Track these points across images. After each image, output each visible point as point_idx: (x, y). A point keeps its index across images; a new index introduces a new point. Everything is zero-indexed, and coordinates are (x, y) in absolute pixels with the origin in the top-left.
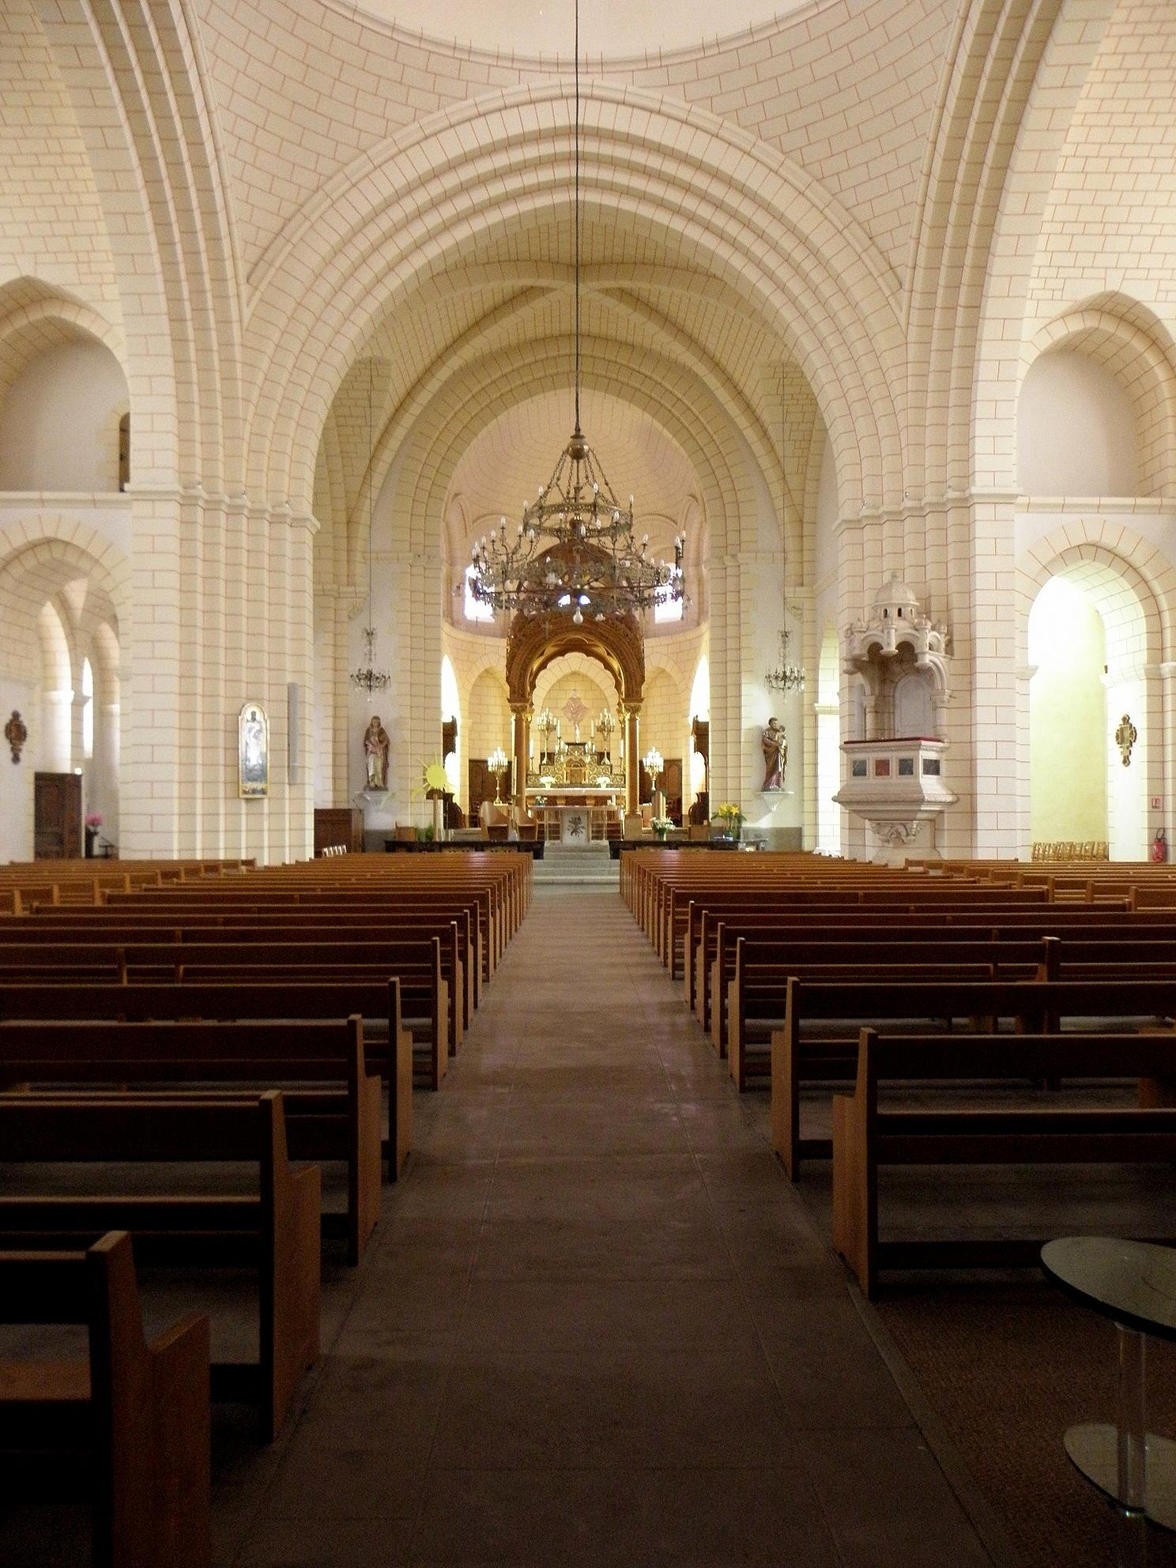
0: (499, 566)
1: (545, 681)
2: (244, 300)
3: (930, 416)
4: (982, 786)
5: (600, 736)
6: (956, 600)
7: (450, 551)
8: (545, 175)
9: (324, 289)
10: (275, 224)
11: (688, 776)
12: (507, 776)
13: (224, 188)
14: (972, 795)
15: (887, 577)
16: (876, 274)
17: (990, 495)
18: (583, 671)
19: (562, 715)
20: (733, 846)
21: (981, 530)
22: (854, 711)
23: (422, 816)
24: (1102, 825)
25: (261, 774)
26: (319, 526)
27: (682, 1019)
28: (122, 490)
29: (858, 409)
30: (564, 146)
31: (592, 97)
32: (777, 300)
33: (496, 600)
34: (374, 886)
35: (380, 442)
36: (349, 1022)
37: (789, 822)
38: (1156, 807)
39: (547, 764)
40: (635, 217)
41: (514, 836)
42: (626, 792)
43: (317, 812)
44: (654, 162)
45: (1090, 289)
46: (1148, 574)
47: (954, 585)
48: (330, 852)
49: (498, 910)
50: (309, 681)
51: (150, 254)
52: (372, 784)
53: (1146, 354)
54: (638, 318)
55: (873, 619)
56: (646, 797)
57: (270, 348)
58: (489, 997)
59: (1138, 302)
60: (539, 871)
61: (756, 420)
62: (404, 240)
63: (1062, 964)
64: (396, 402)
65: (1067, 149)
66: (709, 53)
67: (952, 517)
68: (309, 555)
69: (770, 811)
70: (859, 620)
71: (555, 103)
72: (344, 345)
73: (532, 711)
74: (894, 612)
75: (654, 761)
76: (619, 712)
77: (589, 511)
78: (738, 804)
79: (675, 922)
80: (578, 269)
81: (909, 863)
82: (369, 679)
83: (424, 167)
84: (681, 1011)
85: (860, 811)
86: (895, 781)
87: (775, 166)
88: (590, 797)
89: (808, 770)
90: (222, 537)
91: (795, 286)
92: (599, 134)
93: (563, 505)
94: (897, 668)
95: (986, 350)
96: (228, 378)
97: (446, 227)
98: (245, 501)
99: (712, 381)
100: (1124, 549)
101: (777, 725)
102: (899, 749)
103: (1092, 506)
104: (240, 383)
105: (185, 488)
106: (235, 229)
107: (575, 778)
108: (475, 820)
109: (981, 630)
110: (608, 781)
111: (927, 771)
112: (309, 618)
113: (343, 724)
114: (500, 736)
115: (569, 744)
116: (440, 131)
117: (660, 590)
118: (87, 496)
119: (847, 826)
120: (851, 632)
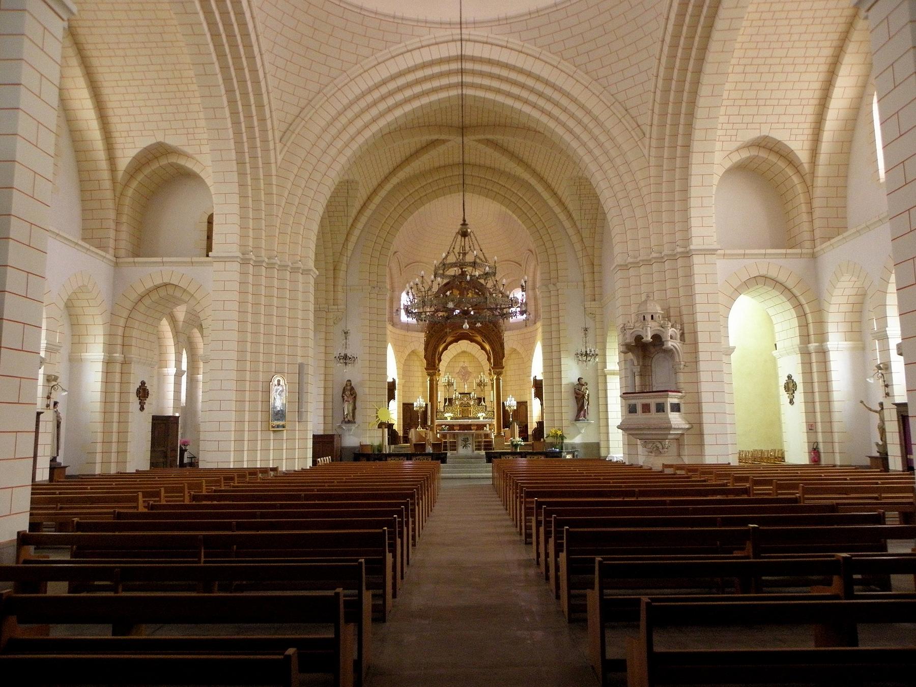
1: (447, 357)
3: (665, 206)
4: (707, 418)
5: (479, 388)
6: (685, 310)
7: (392, 283)
8: (445, 81)
9: (322, 145)
10: (296, 111)
11: (531, 411)
12: (425, 412)
13: (261, 55)
14: (700, 424)
15: (644, 298)
16: (630, 129)
17: (701, 250)
18: (468, 350)
19: (457, 376)
20: (558, 455)
21: (697, 269)
22: (627, 375)
23: (374, 438)
24: (780, 440)
25: (280, 415)
27: (532, 572)
28: (207, 256)
29: (623, 203)
30: (454, 66)
31: (469, 40)
32: (575, 144)
33: (418, 316)
36: (335, 593)
37: (592, 439)
38: (811, 429)
39: (448, 406)
40: (494, 102)
41: (429, 450)
42: (495, 422)
43: (314, 436)
44: (504, 73)
45: (752, 134)
46: (796, 292)
47: (683, 301)
48: (321, 461)
49: (421, 501)
50: (311, 361)
51: (219, 86)
52: (346, 420)
54: (497, 154)
55: (637, 321)
56: (507, 424)
57: (292, 177)
58: (416, 556)
59: (779, 141)
60: (445, 470)
62: (367, 117)
63: (764, 578)
64: (362, 203)
65: (734, 61)
66: (532, 16)
67: (680, 262)
68: (312, 290)
69: (580, 433)
70: (629, 322)
71: (449, 44)
72: (333, 174)
73: (439, 375)
74: (649, 317)
75: (511, 403)
76: (490, 374)
77: (471, 266)
78: (561, 428)
79: (526, 509)
80: (463, 130)
81: (665, 466)
82: (345, 359)
83: (377, 79)
84: (530, 566)
86: (653, 414)
87: (571, 74)
88: (474, 425)
89: (602, 408)
90: (263, 281)
91: (585, 137)
92: (473, 59)
94: (652, 349)
96: (269, 194)
97: (389, 110)
98: (277, 260)
99: (540, 188)
100: (782, 278)
101: (583, 381)
102: (655, 397)
103: (762, 254)
104: (275, 196)
106: (274, 113)
107: (465, 414)
108: (406, 439)
109: (700, 327)
110: (484, 415)
111: (672, 410)
112: (311, 326)
113: (330, 384)
114: (421, 389)
115: (460, 394)
116: (530, 55)
117: (513, 309)
118: (188, 259)
119: (627, 453)
120: (624, 329)
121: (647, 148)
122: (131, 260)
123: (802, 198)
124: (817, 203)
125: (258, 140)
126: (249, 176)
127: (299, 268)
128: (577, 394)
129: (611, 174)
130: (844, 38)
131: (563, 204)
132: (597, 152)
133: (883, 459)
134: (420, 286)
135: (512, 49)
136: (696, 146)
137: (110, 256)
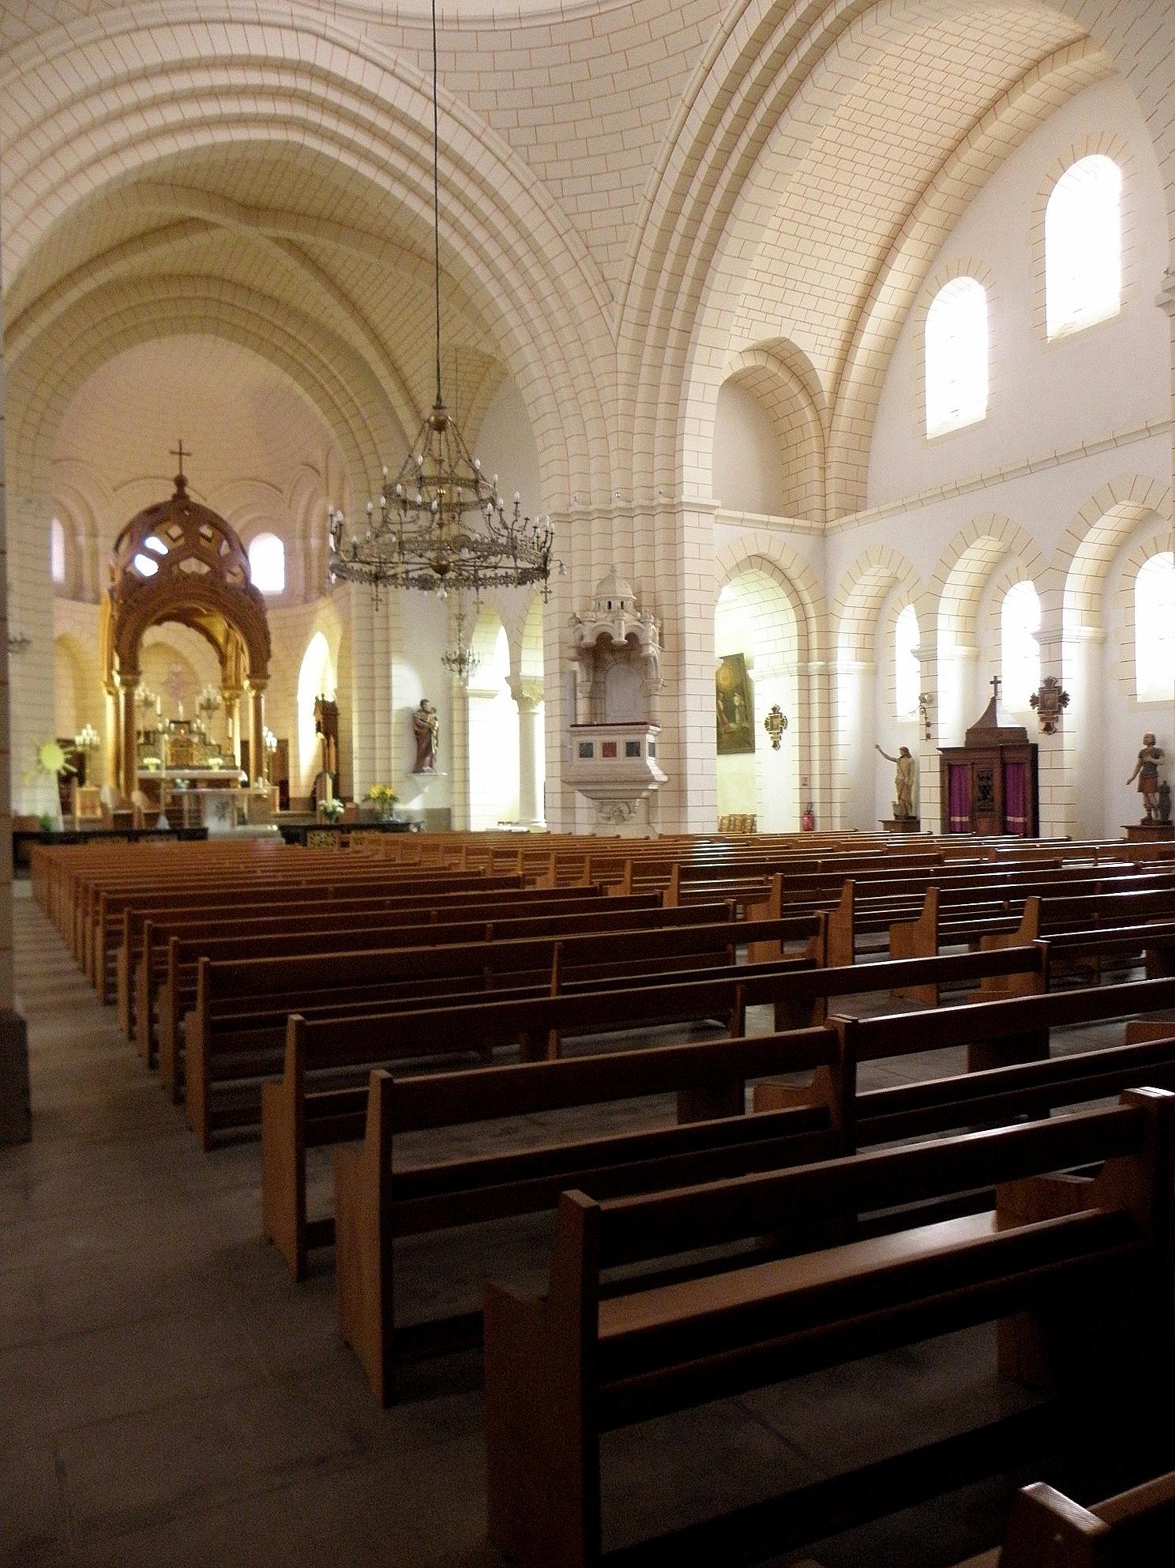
6: (664, 598)
34: (173, 885)
37: (439, 804)
38: (804, 785)
44: (383, 123)
45: (767, 333)
46: (800, 585)
47: (661, 583)
53: (799, 396)
69: (420, 792)
85: (587, 791)
89: (457, 752)
91: (513, 278)
97: (150, 136)
100: (785, 562)
103: (763, 522)
110: (220, 761)
123: (814, 445)
124: (834, 455)
128: (418, 726)
129: (552, 353)
130: (910, 212)
132: (532, 310)
133: (907, 821)
135: (402, 80)
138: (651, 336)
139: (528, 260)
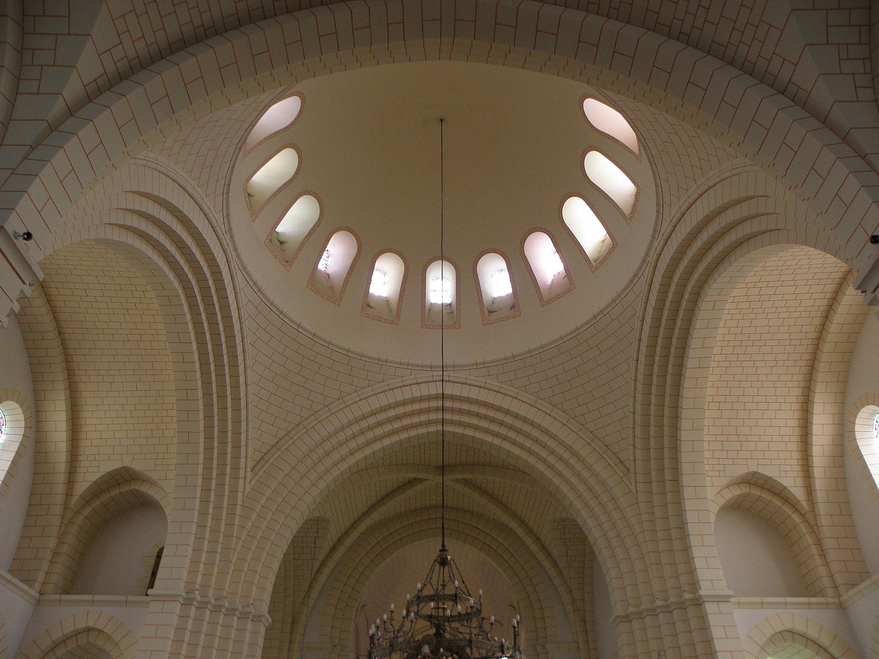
0: (388, 641)
2: (248, 481)
8: (424, 418)
16: (613, 465)
21: (712, 620)
26: (270, 620)
35: (318, 570)
44: (483, 411)
45: (741, 470)
59: (770, 478)
61: (549, 555)
64: (331, 544)
68: (261, 642)
77: (452, 600)
87: (549, 412)
92: (453, 398)
93: (434, 596)
95: (689, 505)
96: (229, 525)
100: (813, 633)
105: (187, 593)
106: (250, 442)
118: (122, 598)
121: (633, 484)
122: (57, 597)
123: (809, 539)
124: (828, 543)
125: (228, 467)
126: (218, 555)
127: (250, 613)
131: (547, 550)
134: (388, 626)
136: (686, 480)
137: (33, 592)
138: (655, 488)
139: (573, 461)
